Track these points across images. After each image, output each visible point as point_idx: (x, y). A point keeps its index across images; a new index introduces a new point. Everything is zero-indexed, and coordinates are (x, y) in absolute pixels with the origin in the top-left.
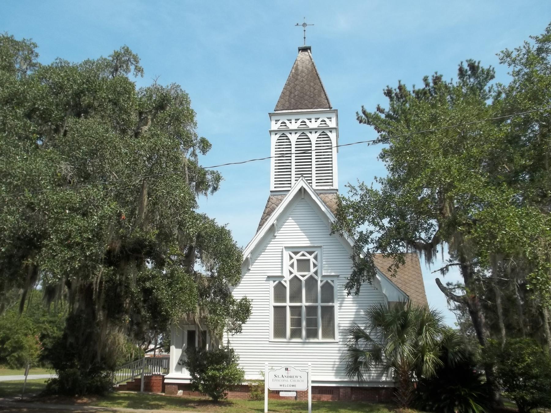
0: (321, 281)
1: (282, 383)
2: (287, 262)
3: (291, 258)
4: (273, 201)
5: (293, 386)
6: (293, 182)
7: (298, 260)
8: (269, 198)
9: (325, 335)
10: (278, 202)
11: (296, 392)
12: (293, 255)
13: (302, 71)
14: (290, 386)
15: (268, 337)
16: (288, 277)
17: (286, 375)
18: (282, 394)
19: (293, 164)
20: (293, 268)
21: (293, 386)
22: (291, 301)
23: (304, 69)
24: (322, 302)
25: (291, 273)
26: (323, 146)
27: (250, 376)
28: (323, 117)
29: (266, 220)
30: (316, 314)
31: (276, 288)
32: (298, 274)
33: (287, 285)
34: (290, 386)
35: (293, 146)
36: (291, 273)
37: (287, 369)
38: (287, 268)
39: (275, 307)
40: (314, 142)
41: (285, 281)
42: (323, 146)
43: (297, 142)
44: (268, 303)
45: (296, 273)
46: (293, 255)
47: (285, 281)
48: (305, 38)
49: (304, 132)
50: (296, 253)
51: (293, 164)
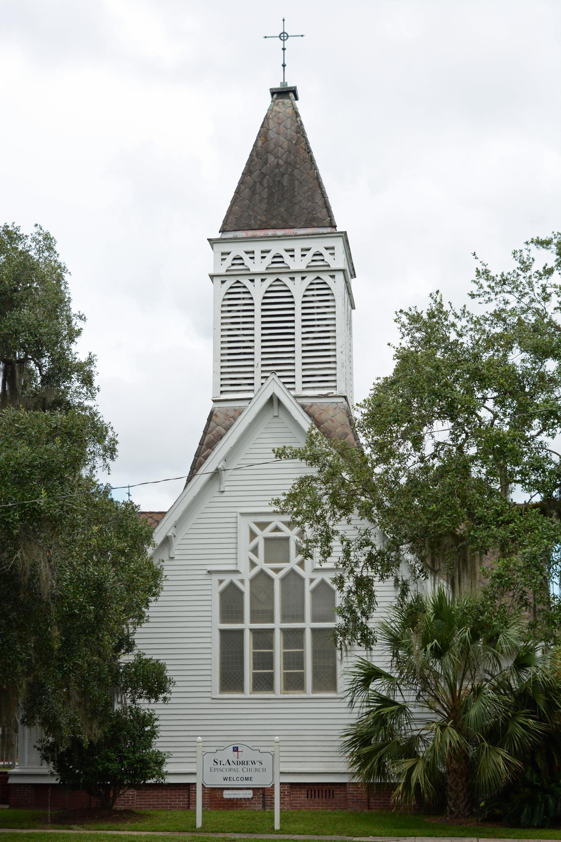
0: (312, 580)
1: (227, 775)
2: (245, 544)
3: (253, 535)
4: (217, 420)
5: (247, 779)
6: (258, 381)
7: (267, 540)
8: (212, 413)
10: (228, 423)
11: (253, 789)
12: (256, 529)
13: (277, 145)
14: (242, 779)
15: (209, 689)
16: (248, 574)
17: (235, 760)
18: (227, 795)
19: (258, 344)
20: (256, 554)
21: (247, 779)
24: (314, 620)
25: (253, 564)
27: (174, 770)
28: (317, 245)
29: (206, 458)
30: (301, 645)
31: (223, 594)
32: (268, 568)
33: (246, 589)
34: (242, 779)
35: (258, 307)
36: (253, 564)
37: (236, 749)
38: (245, 555)
39: (222, 632)
40: (298, 299)
41: (242, 581)
42: (318, 307)
45: (262, 564)
46: (256, 529)
47: (242, 581)
48: (284, 66)
49: (278, 269)
50: (262, 526)
51: (258, 344)
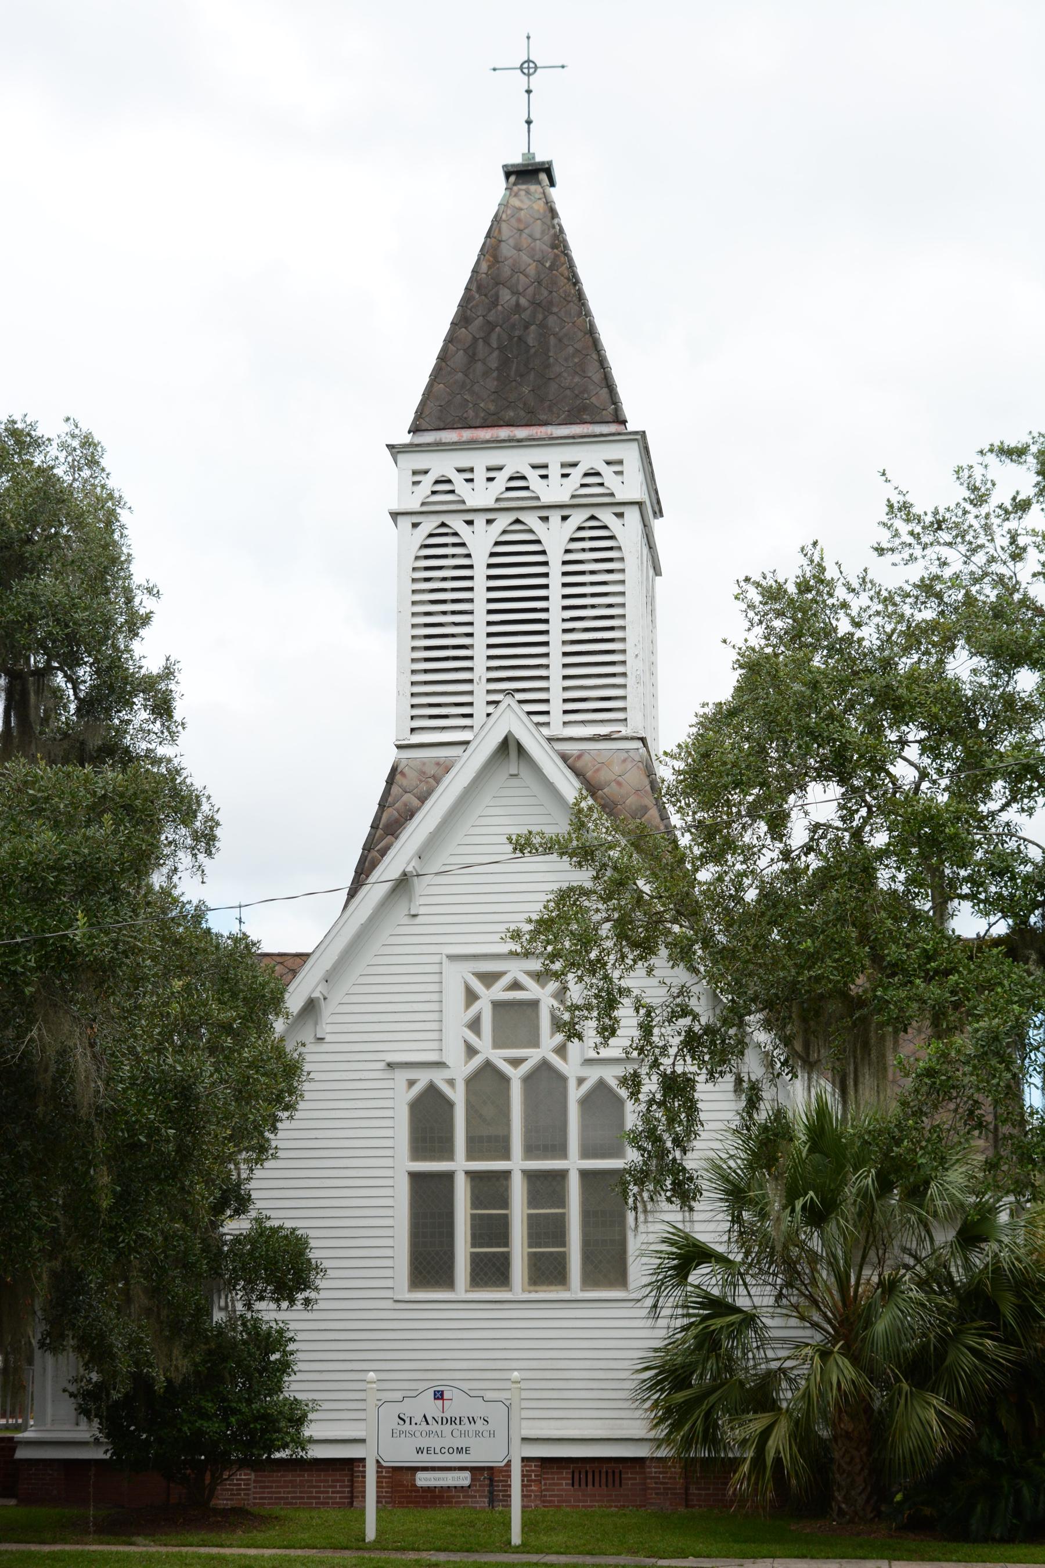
1: (424, 1443)
2: (456, 1015)
3: (471, 996)
4: (405, 782)
5: (460, 1451)
6: (480, 709)
7: (497, 1005)
8: (394, 770)
9: (590, 1279)
10: (425, 787)
11: (472, 1470)
12: (477, 986)
13: (516, 270)
16: (461, 1069)
17: (438, 1415)
18: (423, 1480)
19: (480, 641)
21: (460, 1451)
22: (472, 1154)
23: (525, 258)
25: (471, 1051)
26: (592, 572)
27: (326, 1433)
28: (591, 457)
29: (383, 853)
32: (498, 1057)
33: (458, 1096)
34: (451, 1450)
35: (480, 572)
36: (471, 1051)
37: (439, 1396)
38: (456, 1032)
40: (555, 557)
41: (451, 1082)
43: (493, 555)
44: (389, 1162)
45: (488, 1051)
46: (477, 986)
47: (451, 1082)
48: (529, 122)
49: (518, 501)
50: (489, 979)
51: (480, 641)
